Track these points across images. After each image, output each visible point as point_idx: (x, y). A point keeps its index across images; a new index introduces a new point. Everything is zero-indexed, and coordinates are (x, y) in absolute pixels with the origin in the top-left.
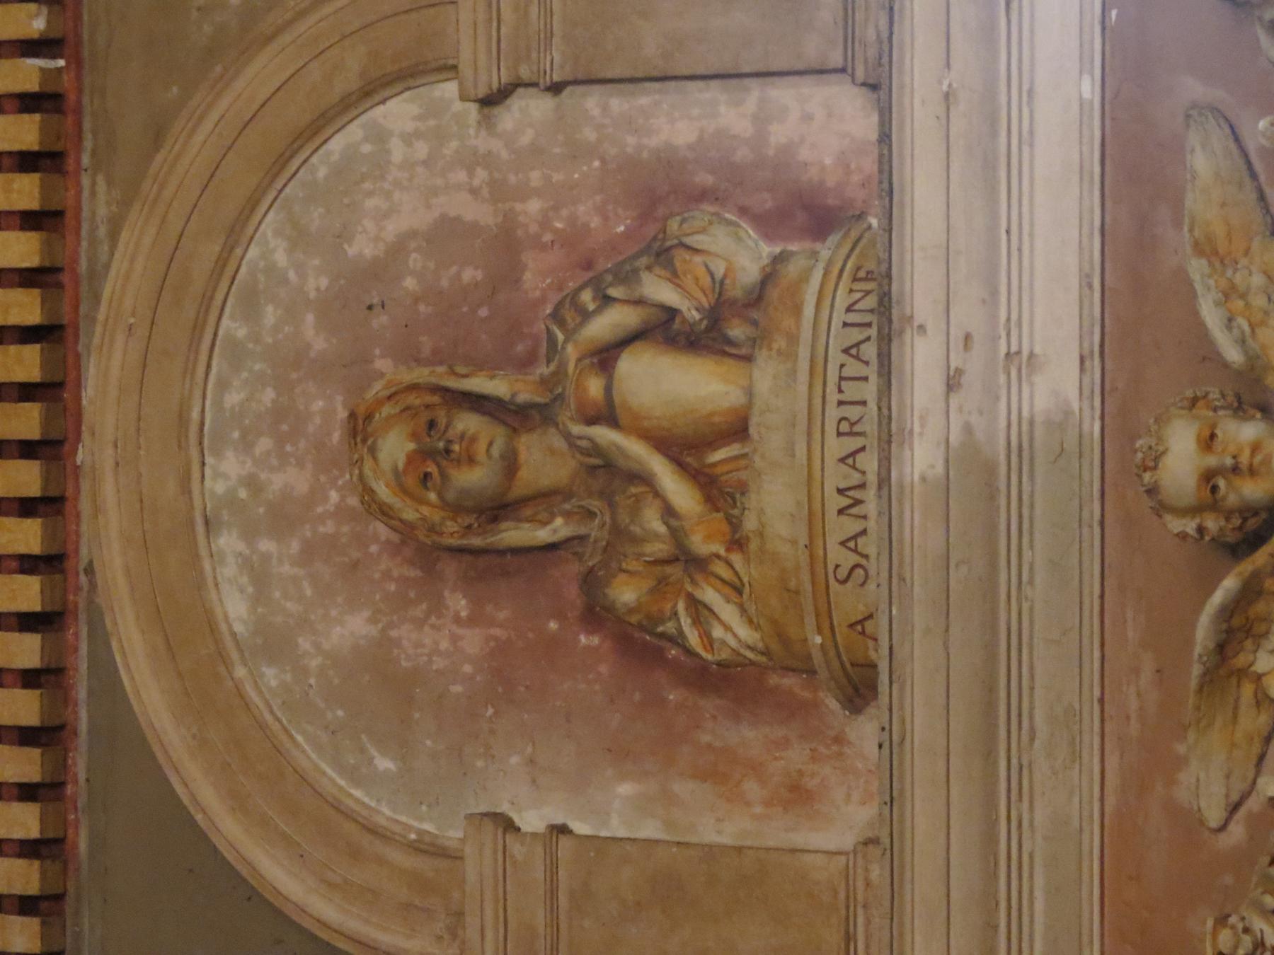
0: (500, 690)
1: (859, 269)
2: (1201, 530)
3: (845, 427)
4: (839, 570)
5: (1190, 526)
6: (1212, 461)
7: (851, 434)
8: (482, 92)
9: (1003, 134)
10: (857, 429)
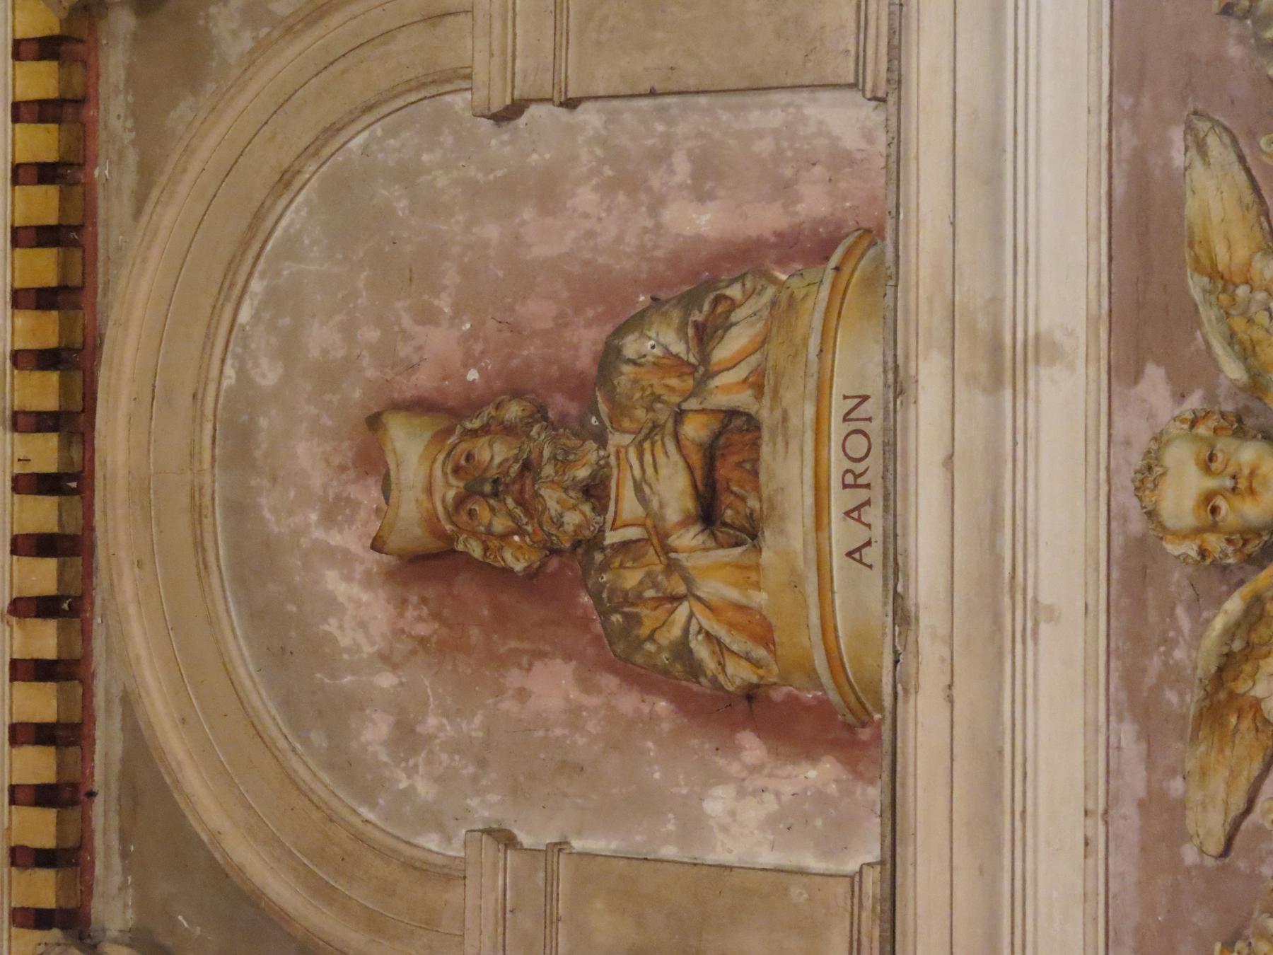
2: (1203, 553)
3: (849, 479)
5: (1190, 548)
6: (1211, 483)
7: (856, 486)
8: (496, 107)
9: (1007, 851)
10: (861, 481)
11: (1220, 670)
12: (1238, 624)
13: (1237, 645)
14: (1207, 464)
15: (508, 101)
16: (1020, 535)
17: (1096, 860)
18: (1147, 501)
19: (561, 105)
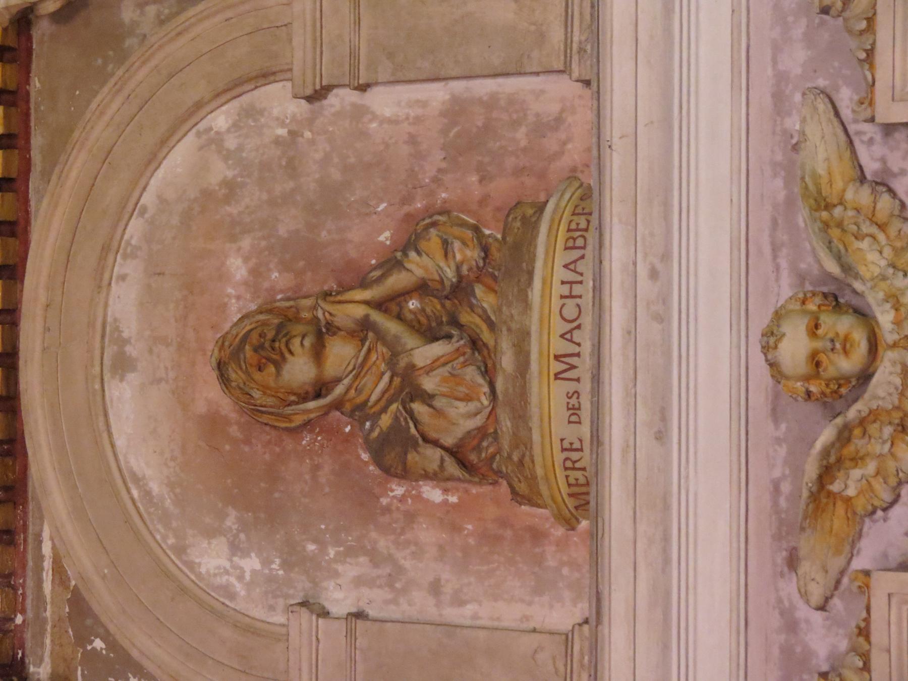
0: (323, 527)
1: (576, 206)
4: (564, 442)
6: (818, 344)
8: (309, 91)
10: (577, 465)
11: (820, 478)
12: (833, 444)
13: (832, 459)
14: (814, 329)
15: (318, 87)
16: (684, 316)
17: (740, 15)
18: (769, 357)
19: (356, 89)
